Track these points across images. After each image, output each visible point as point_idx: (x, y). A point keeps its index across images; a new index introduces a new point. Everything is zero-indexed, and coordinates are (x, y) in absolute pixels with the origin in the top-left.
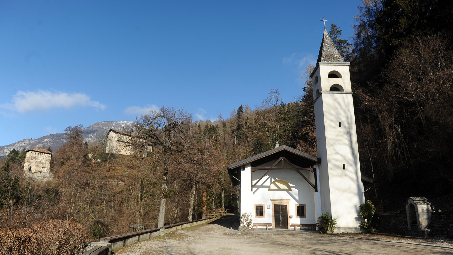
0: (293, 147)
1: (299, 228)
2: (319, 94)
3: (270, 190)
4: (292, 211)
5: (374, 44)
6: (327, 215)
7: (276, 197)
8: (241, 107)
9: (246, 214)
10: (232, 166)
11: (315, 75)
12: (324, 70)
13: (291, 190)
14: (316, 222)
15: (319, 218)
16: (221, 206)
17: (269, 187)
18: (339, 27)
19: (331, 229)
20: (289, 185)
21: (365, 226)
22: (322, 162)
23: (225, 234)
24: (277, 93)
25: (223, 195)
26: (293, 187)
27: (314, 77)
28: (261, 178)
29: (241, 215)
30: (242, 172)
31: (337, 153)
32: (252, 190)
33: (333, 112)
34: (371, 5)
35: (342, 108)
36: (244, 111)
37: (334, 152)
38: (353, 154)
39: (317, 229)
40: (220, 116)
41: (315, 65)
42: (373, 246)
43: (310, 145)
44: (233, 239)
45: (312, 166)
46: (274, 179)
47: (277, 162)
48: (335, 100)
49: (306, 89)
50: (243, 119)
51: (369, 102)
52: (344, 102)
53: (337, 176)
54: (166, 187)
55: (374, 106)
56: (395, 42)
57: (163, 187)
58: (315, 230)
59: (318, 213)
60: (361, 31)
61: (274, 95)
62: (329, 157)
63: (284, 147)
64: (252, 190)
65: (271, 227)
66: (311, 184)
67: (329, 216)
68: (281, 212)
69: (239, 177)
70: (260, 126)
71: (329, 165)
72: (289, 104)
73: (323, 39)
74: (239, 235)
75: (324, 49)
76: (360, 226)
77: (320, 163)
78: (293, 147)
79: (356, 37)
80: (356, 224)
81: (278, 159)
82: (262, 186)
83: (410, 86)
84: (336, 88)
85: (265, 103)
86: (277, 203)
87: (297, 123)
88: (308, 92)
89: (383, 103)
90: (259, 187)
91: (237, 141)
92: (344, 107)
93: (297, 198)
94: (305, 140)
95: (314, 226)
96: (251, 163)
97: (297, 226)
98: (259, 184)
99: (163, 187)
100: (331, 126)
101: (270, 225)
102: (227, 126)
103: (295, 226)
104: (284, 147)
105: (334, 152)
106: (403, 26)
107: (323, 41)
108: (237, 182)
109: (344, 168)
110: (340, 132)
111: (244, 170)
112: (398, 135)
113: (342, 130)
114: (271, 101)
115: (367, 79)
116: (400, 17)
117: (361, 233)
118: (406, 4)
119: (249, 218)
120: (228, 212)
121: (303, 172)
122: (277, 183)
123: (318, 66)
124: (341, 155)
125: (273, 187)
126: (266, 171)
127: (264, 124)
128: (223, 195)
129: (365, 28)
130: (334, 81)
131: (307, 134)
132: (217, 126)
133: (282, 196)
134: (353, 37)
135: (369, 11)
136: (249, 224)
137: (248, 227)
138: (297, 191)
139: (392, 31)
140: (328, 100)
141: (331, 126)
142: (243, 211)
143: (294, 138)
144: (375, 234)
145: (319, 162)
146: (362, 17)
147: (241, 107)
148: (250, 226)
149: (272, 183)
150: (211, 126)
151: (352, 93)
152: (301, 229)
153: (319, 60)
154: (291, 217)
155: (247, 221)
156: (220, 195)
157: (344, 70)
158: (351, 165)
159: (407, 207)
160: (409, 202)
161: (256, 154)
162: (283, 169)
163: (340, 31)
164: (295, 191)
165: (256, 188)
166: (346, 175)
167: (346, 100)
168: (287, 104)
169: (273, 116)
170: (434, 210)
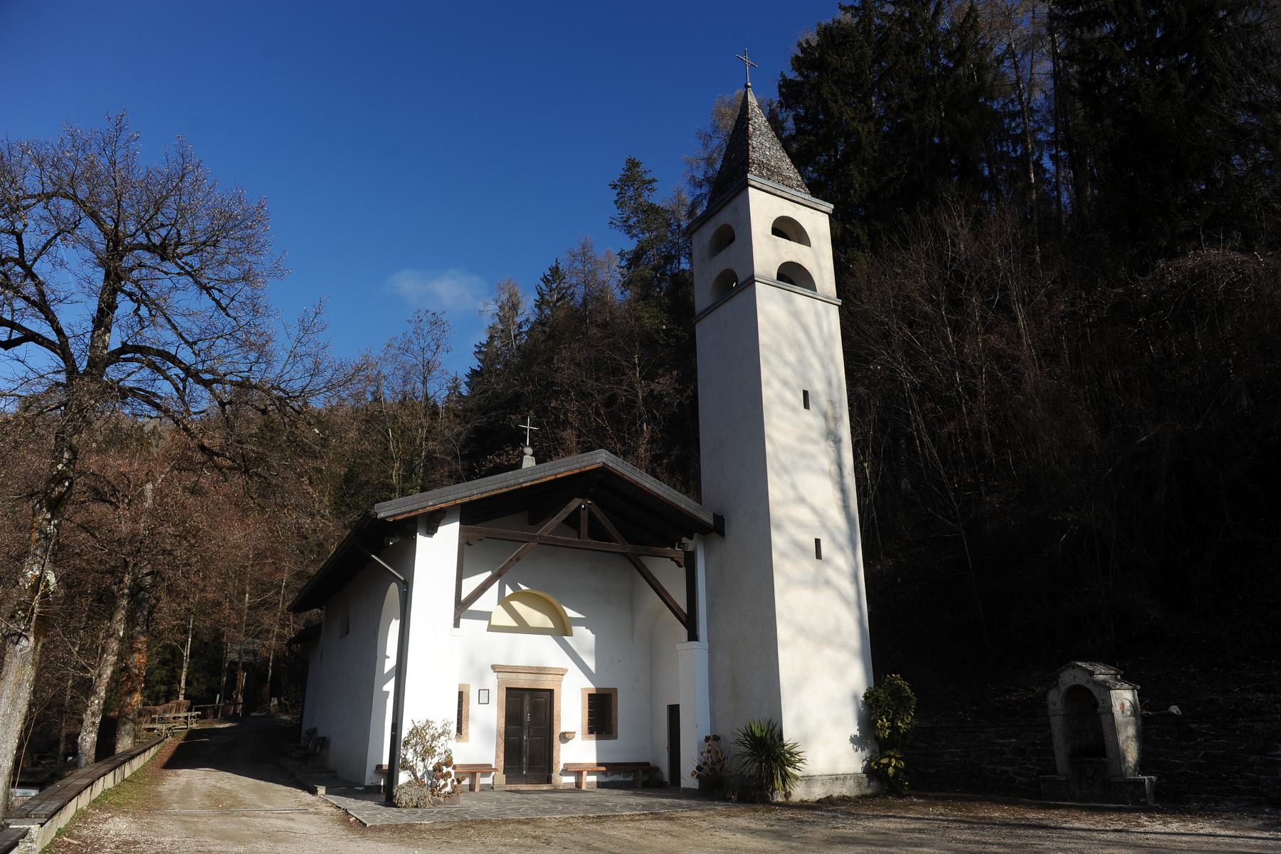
1: (594, 779)
2: (737, 285)
4: (571, 712)
7: (520, 661)
16: (170, 695)
18: (649, 167)
21: (891, 770)
22: (732, 529)
26: (578, 622)
30: (422, 541)
31: (801, 500)
33: (791, 357)
37: (791, 494)
38: (846, 507)
48: (796, 315)
53: (803, 583)
54: (51, 578)
57: (32, 572)
62: (776, 511)
65: (488, 781)
71: (777, 540)
76: (868, 770)
77: (722, 534)
84: (792, 275)
86: (523, 682)
92: (819, 344)
93: (591, 664)
96: (463, 505)
97: (590, 773)
99: (32, 572)
100: (784, 403)
101: (486, 769)
105: (791, 494)
109: (819, 556)
110: (810, 427)
113: (812, 419)
117: (872, 796)
122: (516, 605)
124: (814, 510)
130: (790, 251)
133: (537, 652)
141: (784, 403)
145: (717, 528)
152: (600, 785)
154: (565, 737)
157: (817, 222)
158: (841, 549)
159: (1055, 698)
161: (470, 475)
163: (650, 182)
164: (584, 637)
166: (828, 583)
167: (823, 319)
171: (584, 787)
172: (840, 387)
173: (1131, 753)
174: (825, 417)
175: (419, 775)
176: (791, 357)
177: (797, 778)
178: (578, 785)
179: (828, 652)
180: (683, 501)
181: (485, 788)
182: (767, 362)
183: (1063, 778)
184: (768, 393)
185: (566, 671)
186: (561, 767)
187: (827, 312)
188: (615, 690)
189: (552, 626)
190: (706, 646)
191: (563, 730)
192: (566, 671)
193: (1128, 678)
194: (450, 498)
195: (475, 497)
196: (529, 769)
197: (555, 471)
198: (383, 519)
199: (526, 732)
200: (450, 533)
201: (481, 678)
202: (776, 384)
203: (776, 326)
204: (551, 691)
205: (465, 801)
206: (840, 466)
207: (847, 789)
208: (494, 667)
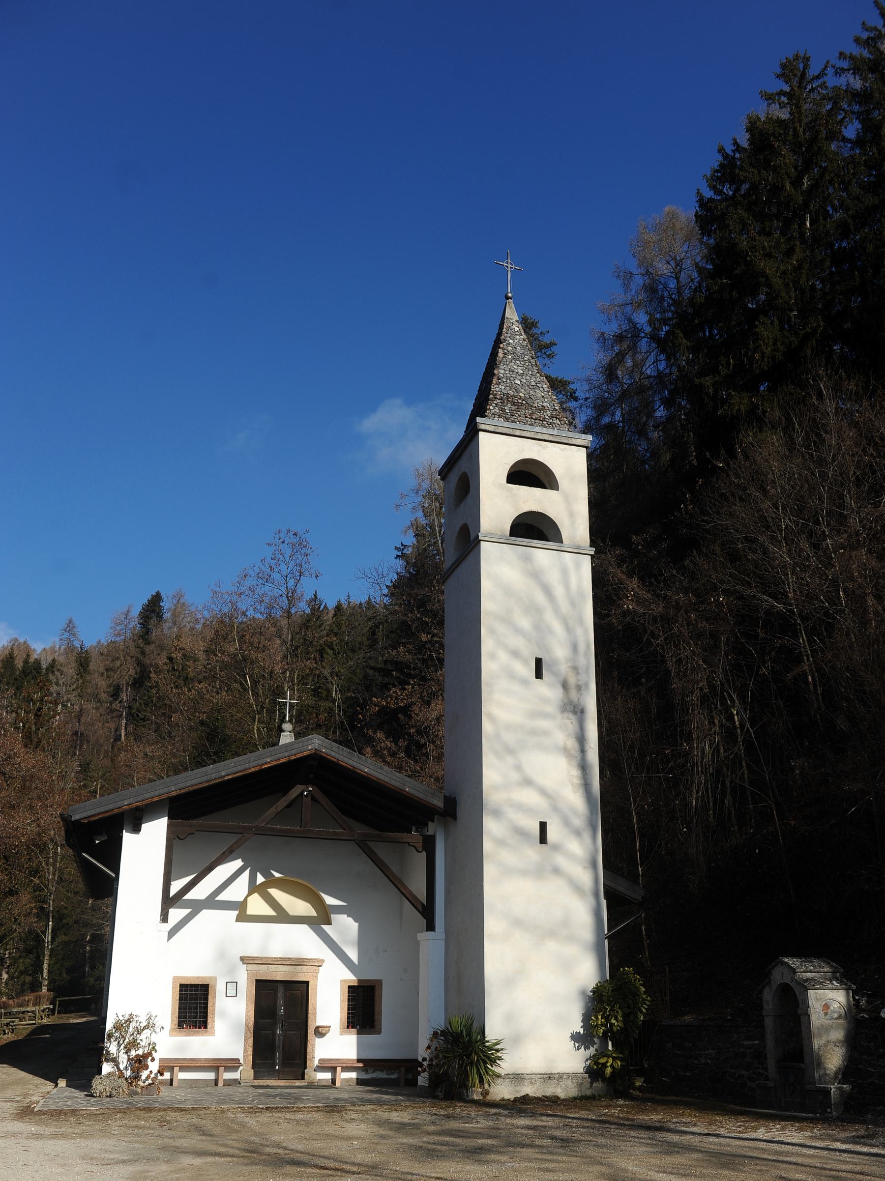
0: (344, 761)
2: (468, 542)
3: (244, 917)
4: (328, 1005)
5: (661, 413)
6: (469, 1028)
7: (276, 951)
8: (156, 599)
9: (129, 1021)
10: (86, 810)
11: (459, 474)
12: (497, 452)
14: (422, 1053)
15: (435, 1034)
17: (240, 907)
19: (481, 1081)
20: (322, 901)
22: (462, 811)
23: (26, 1112)
24: (300, 545)
25: (48, 938)
26: (338, 910)
27: (454, 477)
28: (210, 869)
29: (109, 1026)
30: (128, 838)
31: (528, 782)
32: (164, 918)
34: (663, 268)
35: (556, 610)
36: (167, 616)
37: (515, 776)
38: (586, 786)
39: (423, 1080)
40: (70, 627)
41: (457, 433)
42: (669, 1159)
43: (408, 751)
44: (55, 1136)
45: (422, 825)
47: (283, 802)
48: (536, 575)
49: (408, 551)
50: (162, 648)
51: (638, 603)
53: (524, 873)
55: (655, 619)
56: (740, 402)
58: (413, 1083)
59: (431, 1016)
60: (620, 357)
61: (288, 552)
63: (316, 743)
64: (164, 918)
66: (413, 900)
67: (475, 1026)
68: (280, 1009)
69: (114, 862)
70: (225, 666)
71: (490, 825)
72: (338, 608)
73: (500, 333)
74: (91, 1115)
75: (500, 371)
76: (589, 1071)
77: (454, 817)
78: (344, 761)
79: (599, 378)
80: (573, 1061)
81: (286, 791)
82: (212, 902)
83: (781, 554)
84: (532, 528)
85: (249, 582)
86: (279, 974)
87: (366, 677)
88: (415, 565)
89: (686, 612)
90: (197, 907)
91: (131, 729)
93: (353, 954)
94: (394, 734)
95: (410, 1066)
97: (346, 1069)
98: (200, 892)
100: (512, 675)
101: (232, 1064)
102: (92, 667)
103: (333, 1070)
104: (316, 743)
105: (515, 776)
106: (768, 351)
107: (498, 342)
108: (103, 887)
109: (543, 839)
110: (544, 700)
111: (136, 829)
112: (729, 734)
113: (548, 691)
114: (276, 576)
115: (634, 524)
116: (762, 318)
118: (784, 272)
119: (144, 1038)
120: (65, 1008)
121: (381, 850)
122: (274, 892)
123: (472, 433)
124: (543, 792)
125: (257, 906)
126: (232, 839)
127: (240, 664)
128: (48, 938)
129: (633, 348)
130: (531, 499)
131: (406, 710)
132: (52, 665)
133: (291, 942)
134: (588, 380)
135: (652, 289)
136: (139, 1063)
137: (137, 1077)
138: (356, 925)
139: (728, 363)
140: (502, 571)
141: (512, 675)
142: (119, 1005)
143: (350, 724)
144: (644, 1100)
145: (449, 811)
146: (629, 309)
147: (156, 599)
148: (144, 1074)
149: (253, 888)
150: (26, 662)
151: (592, 551)
152: (360, 1082)
153: (480, 409)
154: (320, 1032)
155: (133, 1053)
156: (39, 940)
157: (569, 461)
158: (578, 833)
159: (768, 995)
160: (778, 976)
162: (304, 836)
163: (549, 346)
164: (345, 927)
165: (183, 912)
166: (557, 871)
168: (331, 605)
169: (275, 656)
170: (863, 1010)
171: (338, 1084)
172: (588, 646)
173: (834, 1060)
174: (565, 686)
175: (122, 1067)
176: (525, 623)
177: (499, 1076)
178: (334, 1081)
179: (552, 945)
180: (409, 786)
181: (229, 1083)
182: (492, 631)
183: (772, 1084)
184: (488, 667)
185: (323, 961)
186: (316, 1063)
187: (578, 566)
188: (380, 982)
189: (314, 914)
190: (443, 936)
191: (318, 1024)
192: (323, 961)
193: (846, 975)
194: (147, 796)
195: (174, 794)
196: (283, 1064)
197: (261, 762)
198: (77, 821)
199: (279, 1025)
200: (156, 830)
201: (232, 970)
202: (503, 656)
203: (508, 591)
204: (307, 983)
205: (165, 1093)
206: (581, 740)
207: (561, 1091)
208: (242, 959)
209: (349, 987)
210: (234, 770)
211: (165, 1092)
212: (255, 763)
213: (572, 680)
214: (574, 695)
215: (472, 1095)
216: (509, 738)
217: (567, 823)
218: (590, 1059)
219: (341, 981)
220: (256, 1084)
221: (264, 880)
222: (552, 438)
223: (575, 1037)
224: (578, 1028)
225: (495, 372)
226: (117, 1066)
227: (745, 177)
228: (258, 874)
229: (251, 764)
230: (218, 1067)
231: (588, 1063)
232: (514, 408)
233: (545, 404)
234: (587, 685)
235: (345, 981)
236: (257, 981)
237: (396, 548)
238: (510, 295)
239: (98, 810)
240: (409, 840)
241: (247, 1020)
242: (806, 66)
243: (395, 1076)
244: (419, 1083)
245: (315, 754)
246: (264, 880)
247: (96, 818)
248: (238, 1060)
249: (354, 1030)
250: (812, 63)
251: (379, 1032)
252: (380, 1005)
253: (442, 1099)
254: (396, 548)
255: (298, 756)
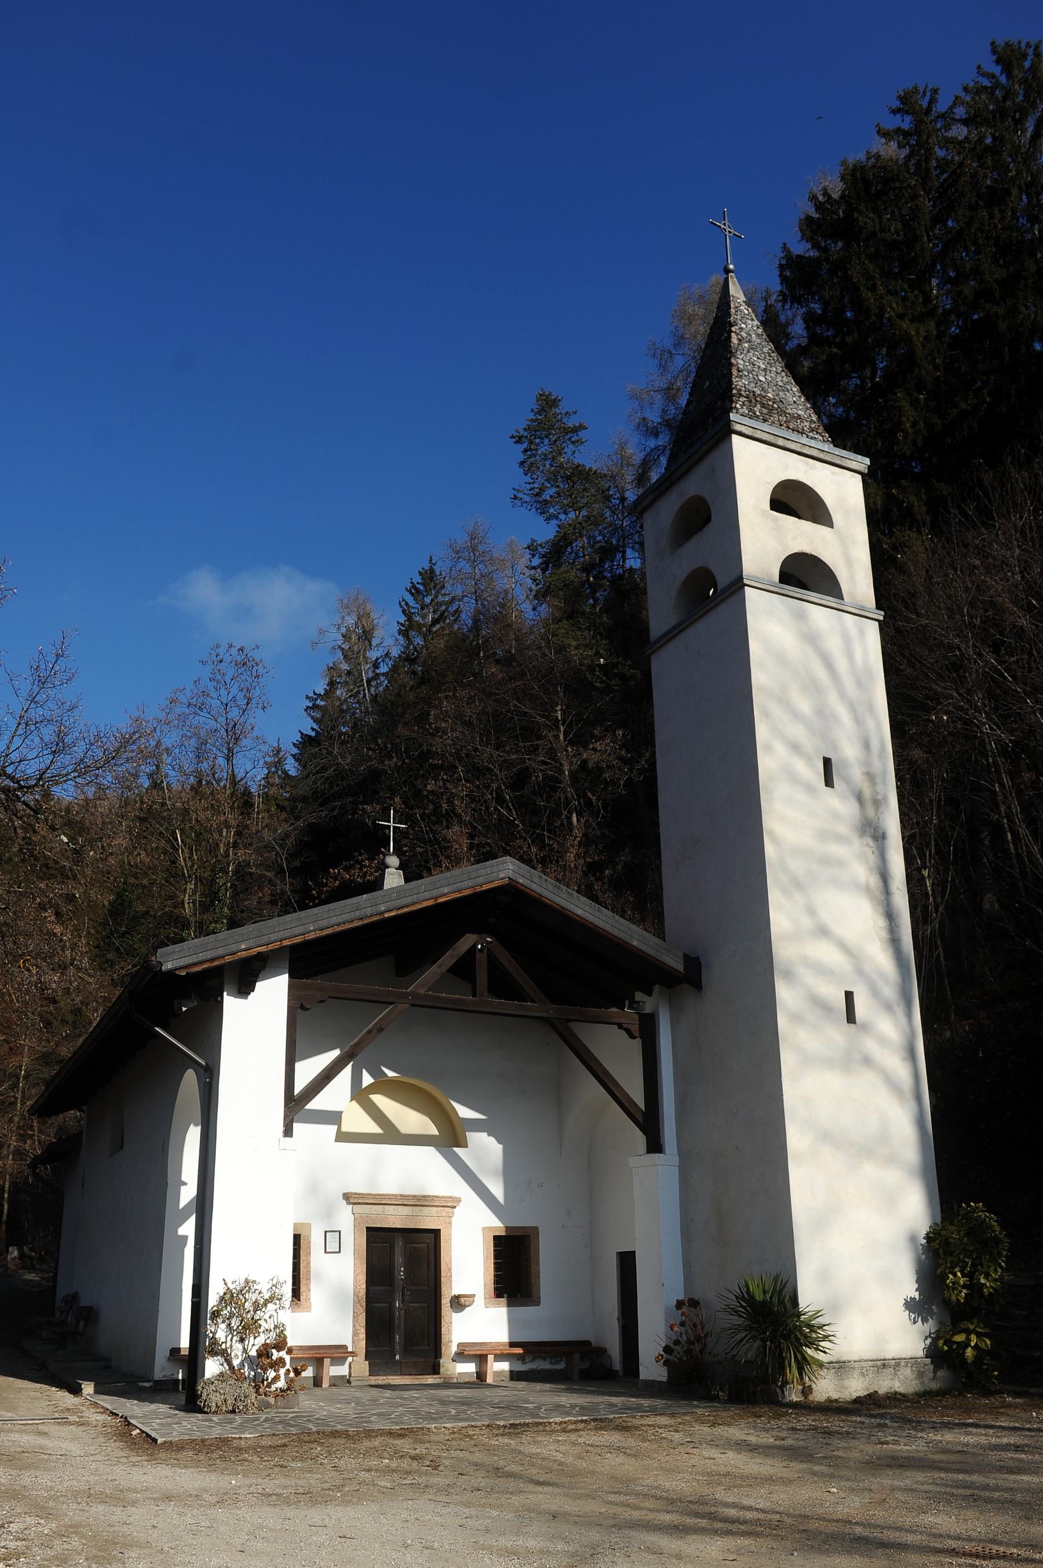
1: (504, 1366)
2: (715, 592)
4: (467, 1264)
7: (389, 1186)
13: (463, 1144)
18: (574, 406)
22: (714, 977)
26: (475, 1126)
30: (230, 1003)
31: (823, 932)
33: (805, 706)
35: (842, 693)
37: (807, 922)
38: (894, 941)
46: (376, 1073)
48: (811, 639)
52: (850, 657)
53: (828, 1063)
65: (342, 1370)
71: (785, 995)
84: (804, 575)
86: (395, 1218)
93: (498, 1190)
96: (293, 948)
97: (499, 1358)
100: (793, 778)
101: (338, 1353)
109: (851, 1018)
110: (835, 816)
113: (838, 804)
122: (380, 1100)
124: (844, 947)
130: (800, 536)
133: (414, 1171)
138: (499, 1148)
141: (793, 778)
145: (690, 977)
154: (459, 1303)
157: (842, 487)
158: (888, 1007)
163: (576, 430)
164: (485, 1149)
166: (867, 1061)
171: (489, 1380)
174: (860, 798)
175: (236, 1363)
176: (805, 706)
177: (821, 1365)
178: (481, 1375)
179: (869, 1169)
180: (634, 935)
181: (336, 1382)
182: (766, 714)
185: (459, 1200)
186: (454, 1349)
187: (862, 632)
191: (456, 1292)
192: (459, 1200)
195: (312, 936)
196: (406, 1352)
197: (435, 893)
199: (398, 1296)
200: (273, 992)
201: (329, 1213)
202: (781, 749)
203: (781, 659)
204: (437, 1233)
206: (884, 876)
207: (902, 1383)
208: (347, 1197)
209: (495, 1238)
210: (398, 903)
211: (307, 1402)
212: (427, 895)
213: (867, 793)
214: (871, 812)
215: (790, 1395)
216: (796, 866)
217: (875, 993)
218: (930, 1336)
219: (484, 1229)
220: (373, 1383)
221: (372, 1081)
222: (821, 456)
223: (910, 1305)
224: (911, 1290)
225: (733, 361)
226: (229, 1362)
227: (865, 223)
228: (364, 1071)
229: (422, 896)
230: (322, 1359)
231: (928, 1342)
232: (765, 411)
233: (800, 412)
234: (885, 798)
235: (489, 1228)
236: (369, 1230)
237: (307, 697)
238: (731, 267)
239: (201, 957)
240: (621, 1021)
241: (355, 1287)
242: (932, 101)
243: (561, 1366)
244: (642, 1377)
245: (508, 885)
246: (372, 1081)
247: (199, 968)
248: (345, 1347)
249: (504, 1300)
250: (940, 97)
251: (537, 1303)
252: (538, 1264)
253: (726, 1402)
254: (307, 697)
255: (485, 887)
